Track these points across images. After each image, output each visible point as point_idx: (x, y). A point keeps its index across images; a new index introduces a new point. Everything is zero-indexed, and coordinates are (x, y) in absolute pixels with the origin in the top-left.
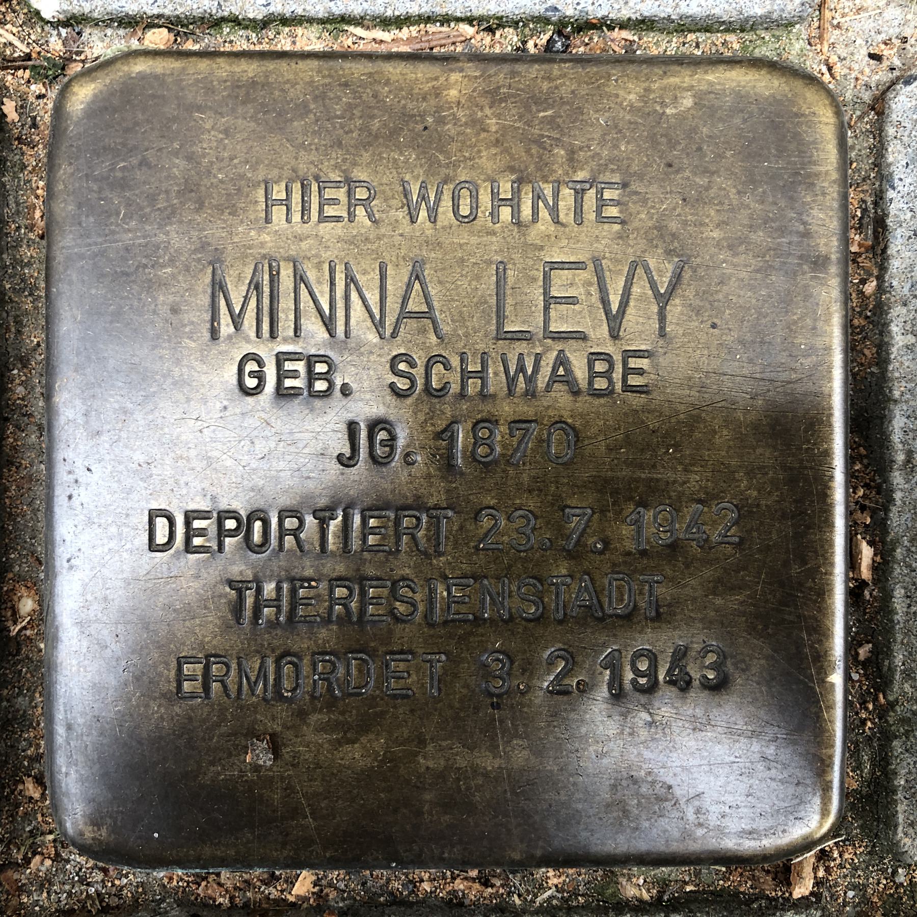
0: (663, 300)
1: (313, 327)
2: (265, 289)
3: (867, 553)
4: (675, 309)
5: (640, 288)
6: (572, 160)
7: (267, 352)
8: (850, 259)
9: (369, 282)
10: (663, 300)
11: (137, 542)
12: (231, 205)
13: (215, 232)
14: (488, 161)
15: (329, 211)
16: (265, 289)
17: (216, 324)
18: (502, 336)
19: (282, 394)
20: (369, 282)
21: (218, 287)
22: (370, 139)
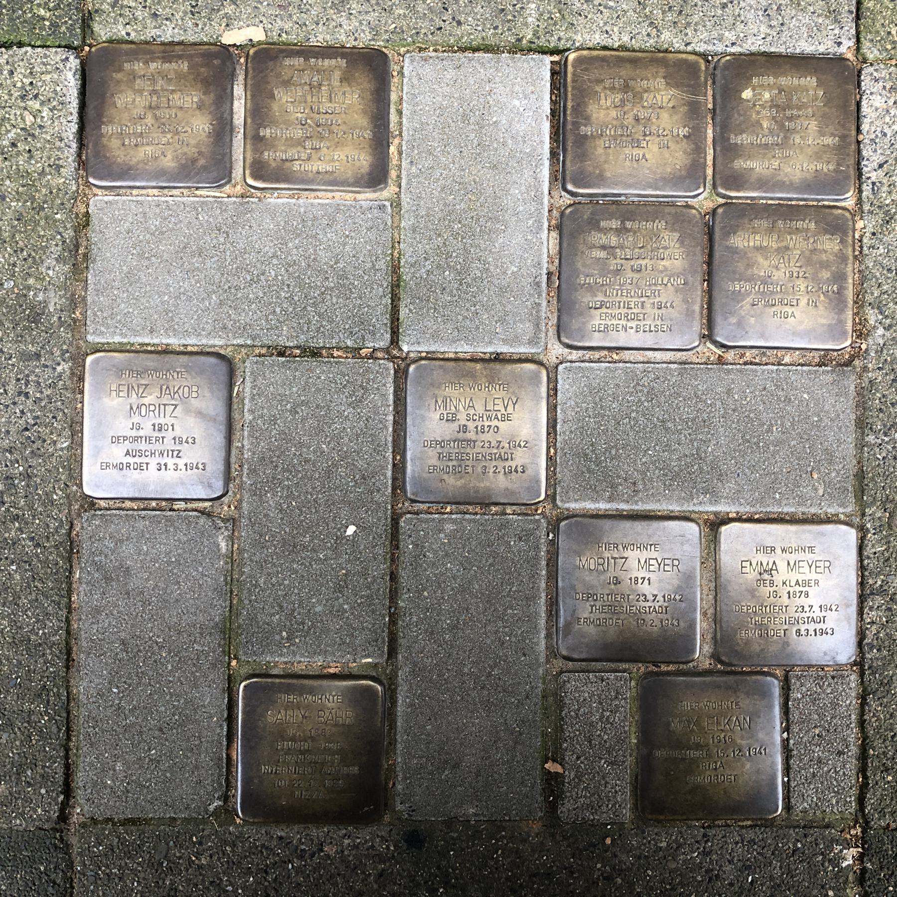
0: (514, 404)
1: (453, 408)
2: (445, 402)
3: (552, 451)
4: (516, 406)
5: (510, 402)
6: (499, 380)
7: (445, 413)
8: (548, 396)
9: (463, 400)
10: (514, 404)
11: (193, 492)
12: (439, 387)
13: (436, 392)
14: (484, 380)
15: (667, 568)
16: (445, 402)
17: (756, 517)
18: (486, 410)
19: (447, 420)
20: (463, 400)
21: (437, 401)
22: (463, 376)
